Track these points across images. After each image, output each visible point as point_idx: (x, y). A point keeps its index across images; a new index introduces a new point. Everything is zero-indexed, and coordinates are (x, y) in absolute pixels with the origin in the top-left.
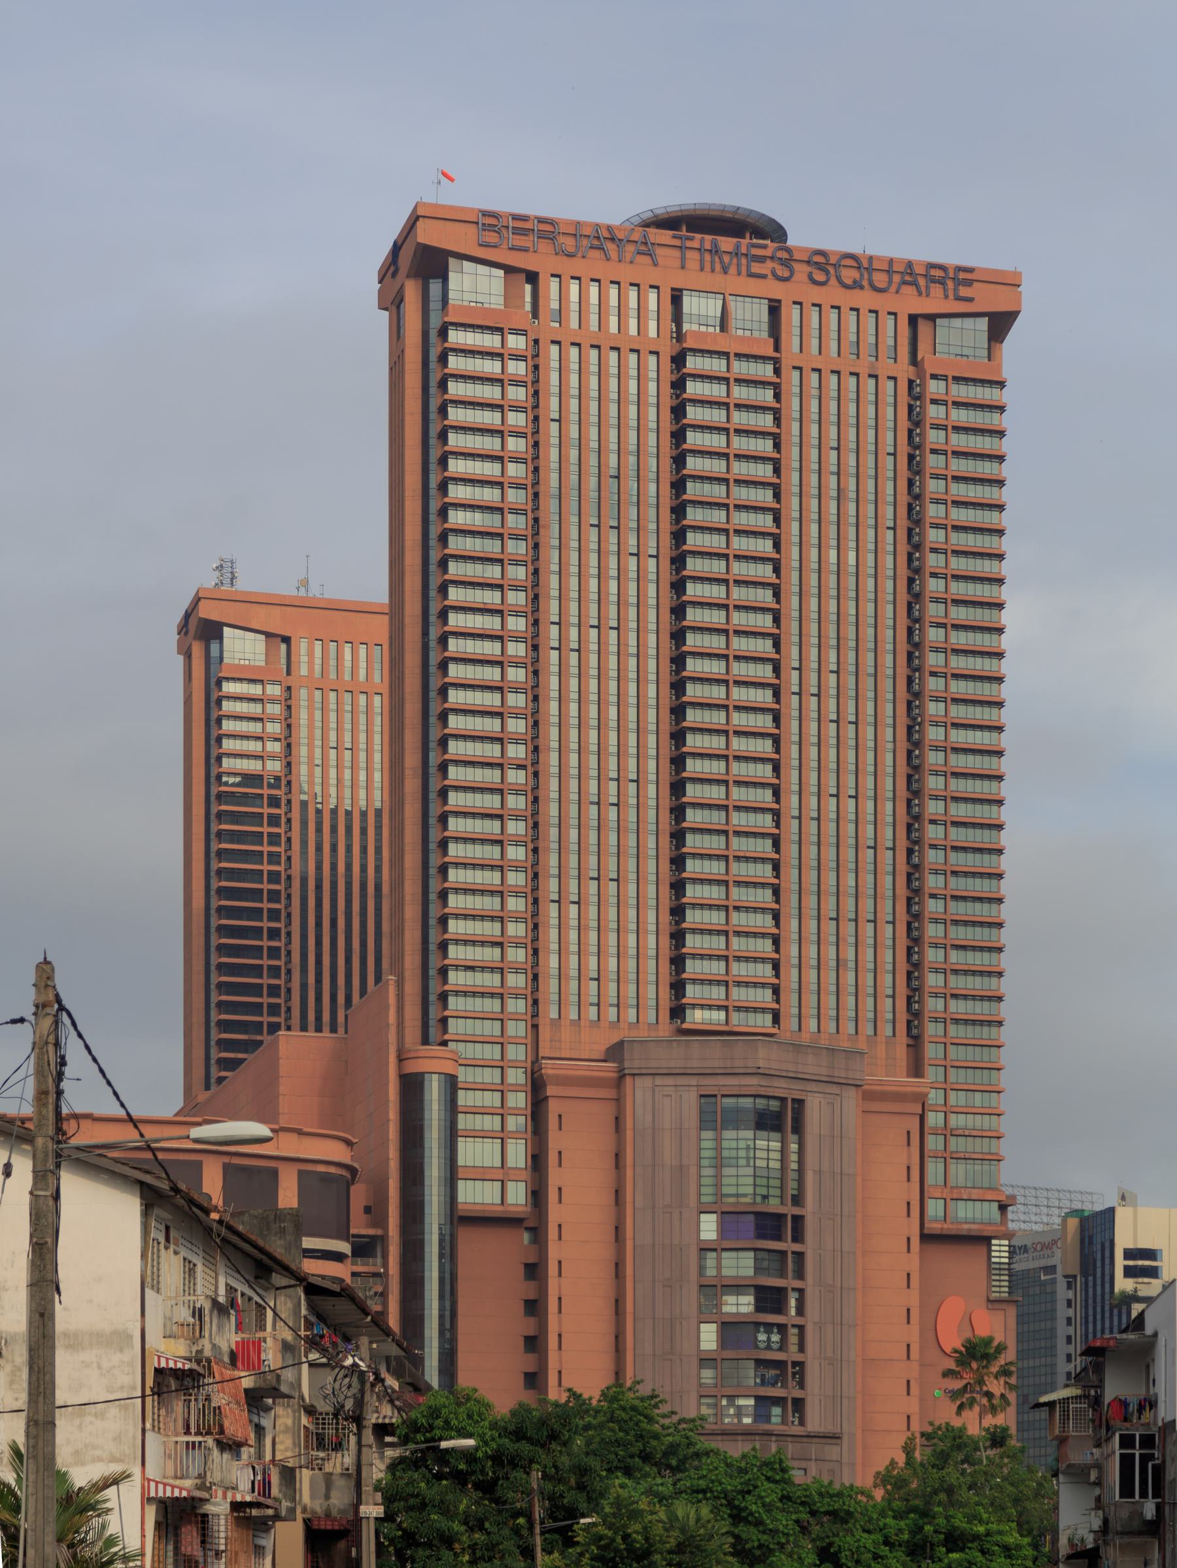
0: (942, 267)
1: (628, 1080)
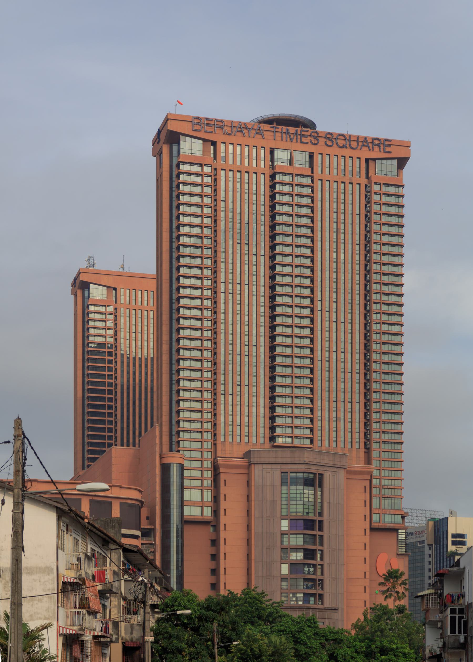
1: (253, 466)
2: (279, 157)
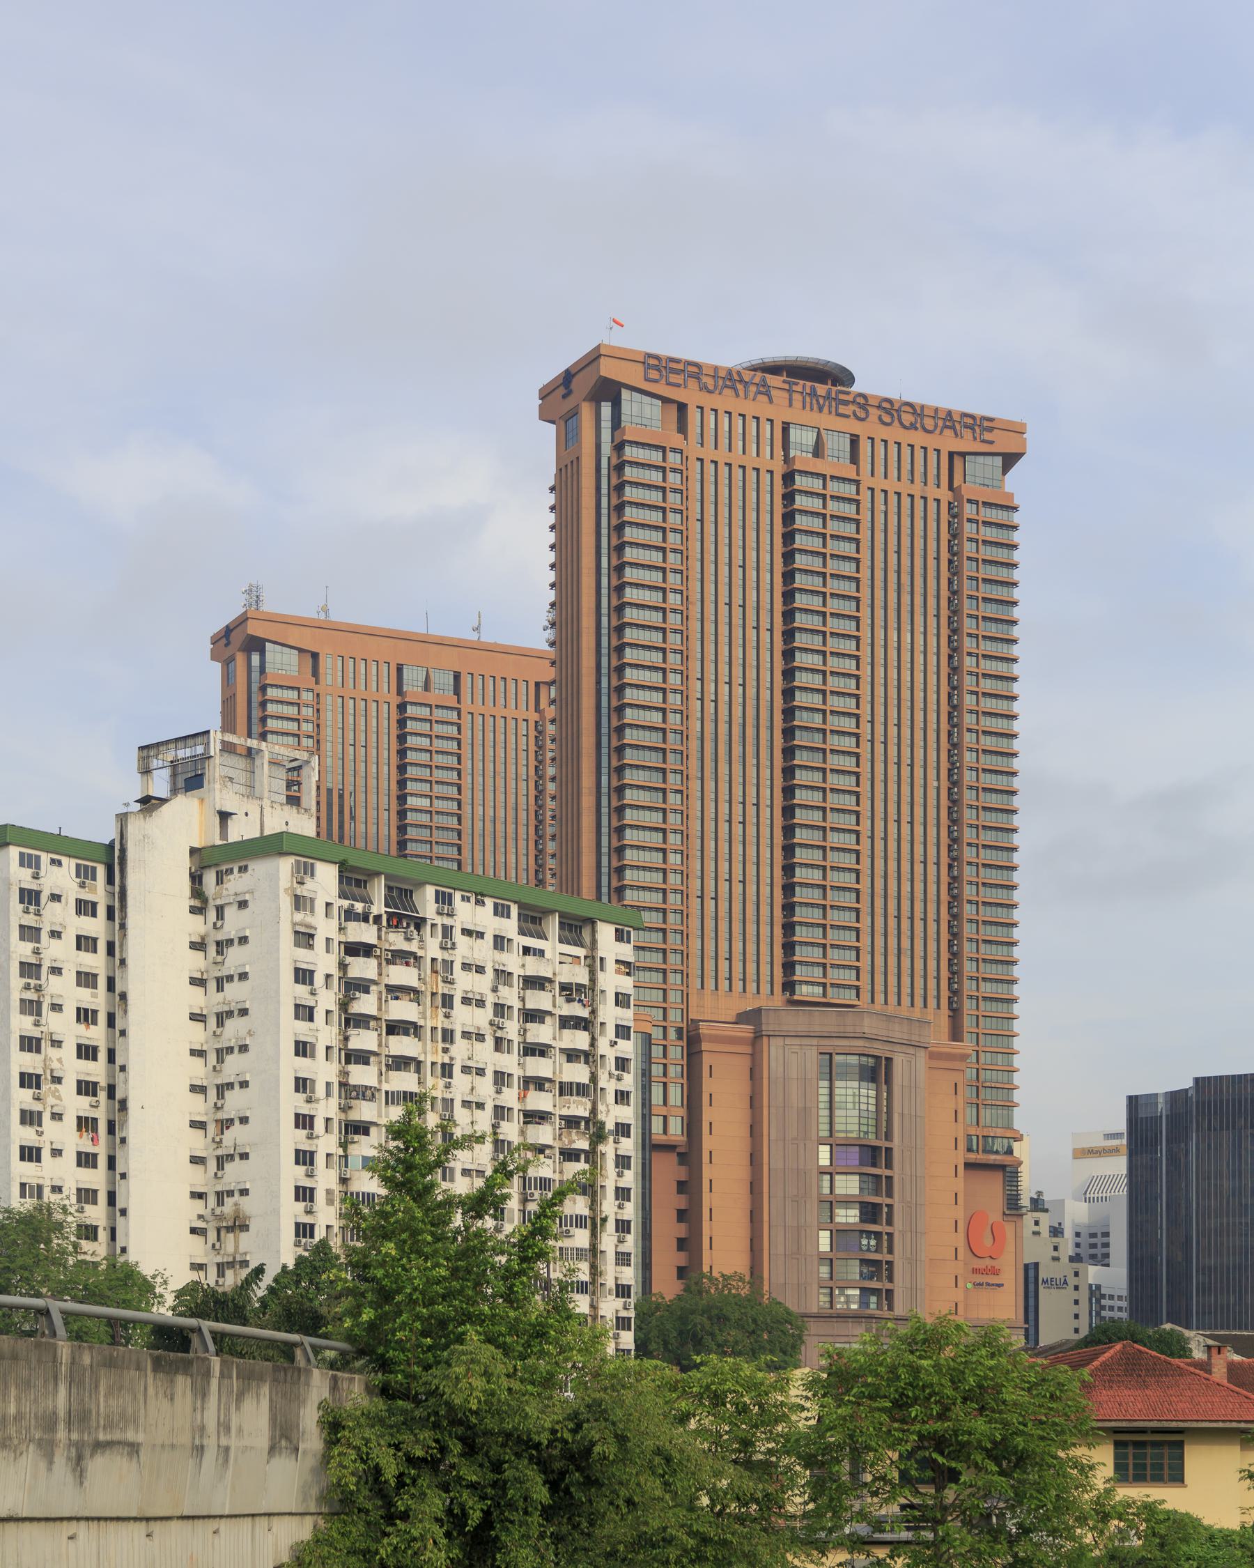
0: (678, 361)
1: (765, 1039)
2: (798, 441)
